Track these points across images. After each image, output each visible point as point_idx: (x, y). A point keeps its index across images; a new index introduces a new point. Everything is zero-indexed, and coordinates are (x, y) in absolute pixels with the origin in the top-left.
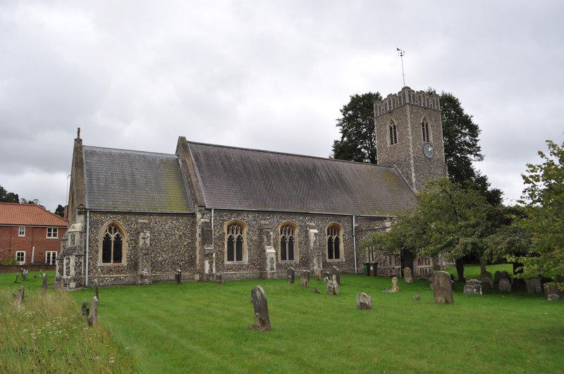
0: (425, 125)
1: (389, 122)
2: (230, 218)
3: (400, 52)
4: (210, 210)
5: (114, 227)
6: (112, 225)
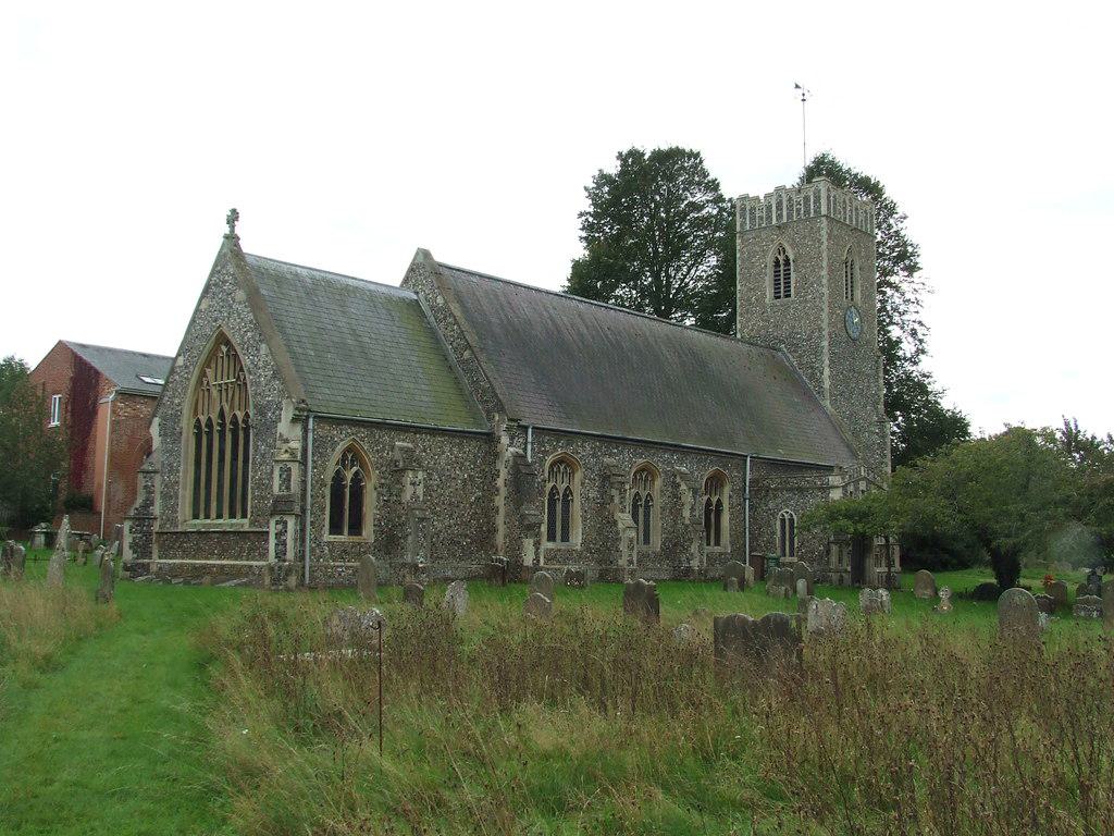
0: (849, 264)
1: (773, 248)
2: (555, 449)
3: (800, 91)
4: (526, 428)
5: (352, 455)
6: (349, 449)
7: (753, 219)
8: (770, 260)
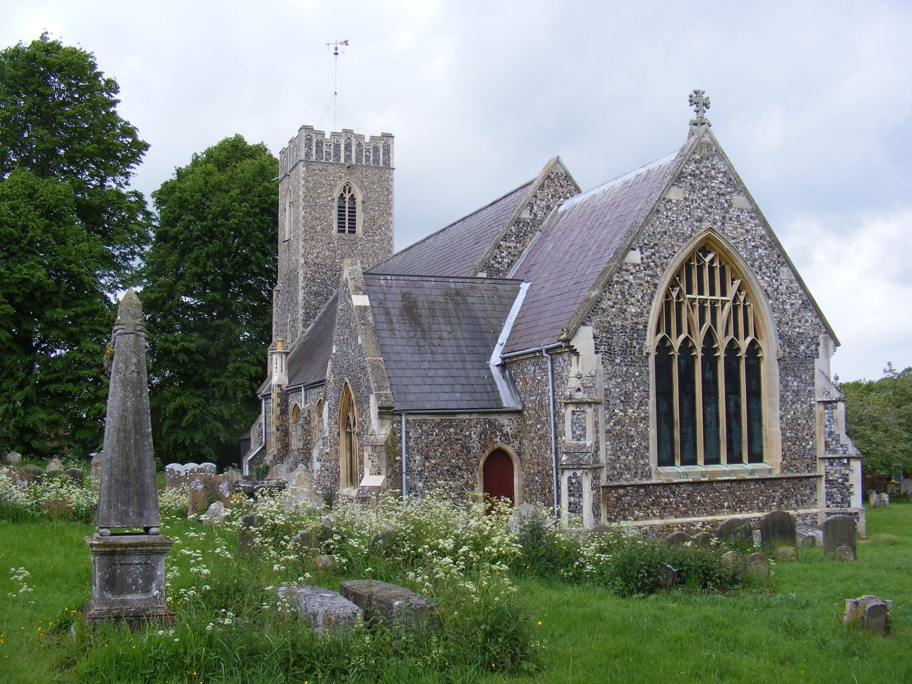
1: (340, 185)
3: (341, 48)
7: (319, 150)
8: (336, 195)
